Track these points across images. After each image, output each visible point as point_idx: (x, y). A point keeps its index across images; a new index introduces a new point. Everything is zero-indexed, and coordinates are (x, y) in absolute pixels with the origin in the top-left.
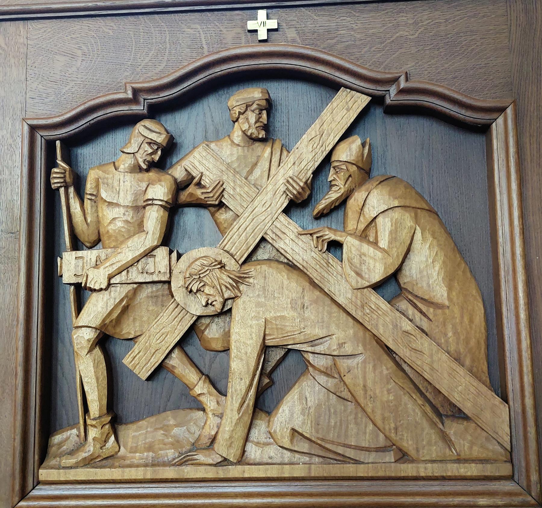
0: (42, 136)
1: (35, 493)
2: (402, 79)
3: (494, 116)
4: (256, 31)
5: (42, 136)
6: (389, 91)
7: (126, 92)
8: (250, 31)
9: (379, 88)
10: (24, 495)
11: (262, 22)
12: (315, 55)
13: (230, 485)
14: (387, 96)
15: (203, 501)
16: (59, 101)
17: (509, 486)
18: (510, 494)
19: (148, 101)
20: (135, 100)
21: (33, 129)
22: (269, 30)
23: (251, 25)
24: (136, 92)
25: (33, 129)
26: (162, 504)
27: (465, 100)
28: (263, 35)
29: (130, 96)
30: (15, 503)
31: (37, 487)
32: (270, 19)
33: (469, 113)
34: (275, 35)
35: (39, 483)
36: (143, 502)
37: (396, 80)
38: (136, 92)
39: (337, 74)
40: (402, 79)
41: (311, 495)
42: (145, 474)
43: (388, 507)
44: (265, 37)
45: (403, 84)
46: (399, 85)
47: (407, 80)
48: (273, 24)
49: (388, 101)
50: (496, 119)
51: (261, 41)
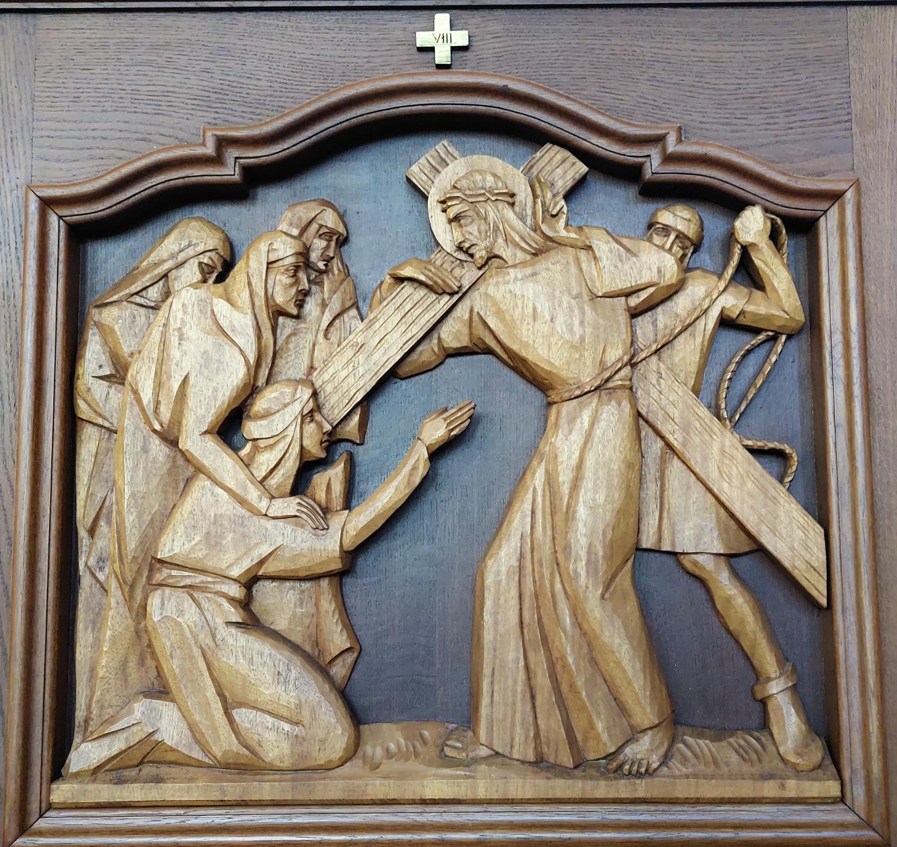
0: (60, 217)
1: (42, 824)
2: (671, 140)
3: (823, 206)
4: (432, 49)
6: (649, 156)
7: (204, 144)
8: (421, 50)
10: (24, 828)
11: (442, 34)
13: (293, 811)
14: (648, 164)
16: (86, 166)
17: (839, 814)
18: (843, 826)
19: (242, 161)
20: (217, 160)
21: (47, 204)
22: (454, 49)
23: (423, 39)
24: (223, 143)
25: (47, 204)
26: (788, 840)
27: (782, 179)
28: (442, 55)
29: (209, 150)
30: (10, 839)
31: (48, 814)
34: (459, 54)
35: (50, 807)
36: (674, 835)
37: (659, 140)
38: (223, 143)
42: (583, 790)
45: (672, 146)
46: (664, 149)
47: (679, 141)
48: (461, 38)
49: (648, 175)
50: (826, 211)
51: (440, 67)
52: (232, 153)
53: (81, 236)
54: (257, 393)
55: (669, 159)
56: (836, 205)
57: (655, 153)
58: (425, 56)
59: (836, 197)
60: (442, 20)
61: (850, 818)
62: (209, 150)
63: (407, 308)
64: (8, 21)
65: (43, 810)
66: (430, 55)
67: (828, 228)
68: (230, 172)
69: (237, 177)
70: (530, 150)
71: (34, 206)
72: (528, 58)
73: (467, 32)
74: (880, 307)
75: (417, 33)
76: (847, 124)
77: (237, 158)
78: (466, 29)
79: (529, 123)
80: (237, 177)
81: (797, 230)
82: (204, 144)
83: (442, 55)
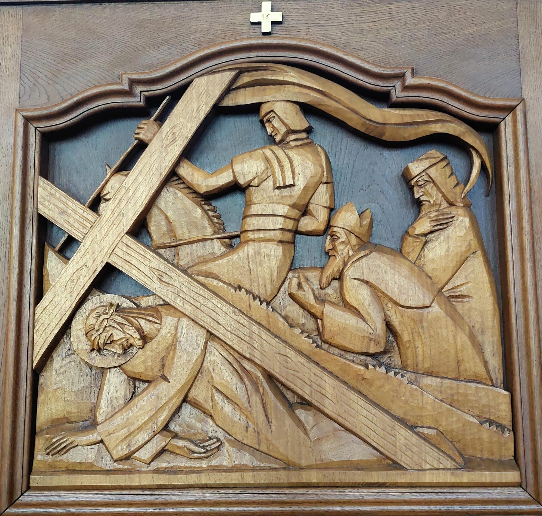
0: (36, 128)
1: (23, 499)
2: (409, 74)
3: (502, 115)
4: (259, 23)
5: (36, 128)
6: (394, 86)
7: (121, 83)
8: (253, 23)
9: (381, 84)
10: (12, 503)
12: (360, 64)
19: (144, 93)
20: (129, 93)
21: (28, 120)
23: (255, 17)
25: (28, 120)
28: (266, 28)
29: (126, 88)
31: (27, 493)
33: (469, 110)
34: (277, 27)
35: (28, 488)
37: (401, 76)
38: (133, 82)
39: (324, 61)
40: (409, 74)
43: (1, 464)
44: (269, 30)
45: (410, 81)
46: (404, 81)
47: (413, 75)
48: (278, 17)
49: (394, 98)
50: (504, 118)
51: (264, 34)
52: (138, 89)
53: (49, 139)
54: (287, 406)
55: (406, 88)
56: (511, 114)
57: (398, 84)
59: (511, 109)
61: (525, 496)
62: (126, 87)
65: (24, 490)
66: (259, 26)
67: (506, 130)
68: (138, 100)
69: (142, 104)
70: (323, 126)
71: (34, 138)
74: (535, 187)
75: (251, 14)
77: (141, 91)
80: (142, 104)
81: (489, 129)
82: (121, 83)
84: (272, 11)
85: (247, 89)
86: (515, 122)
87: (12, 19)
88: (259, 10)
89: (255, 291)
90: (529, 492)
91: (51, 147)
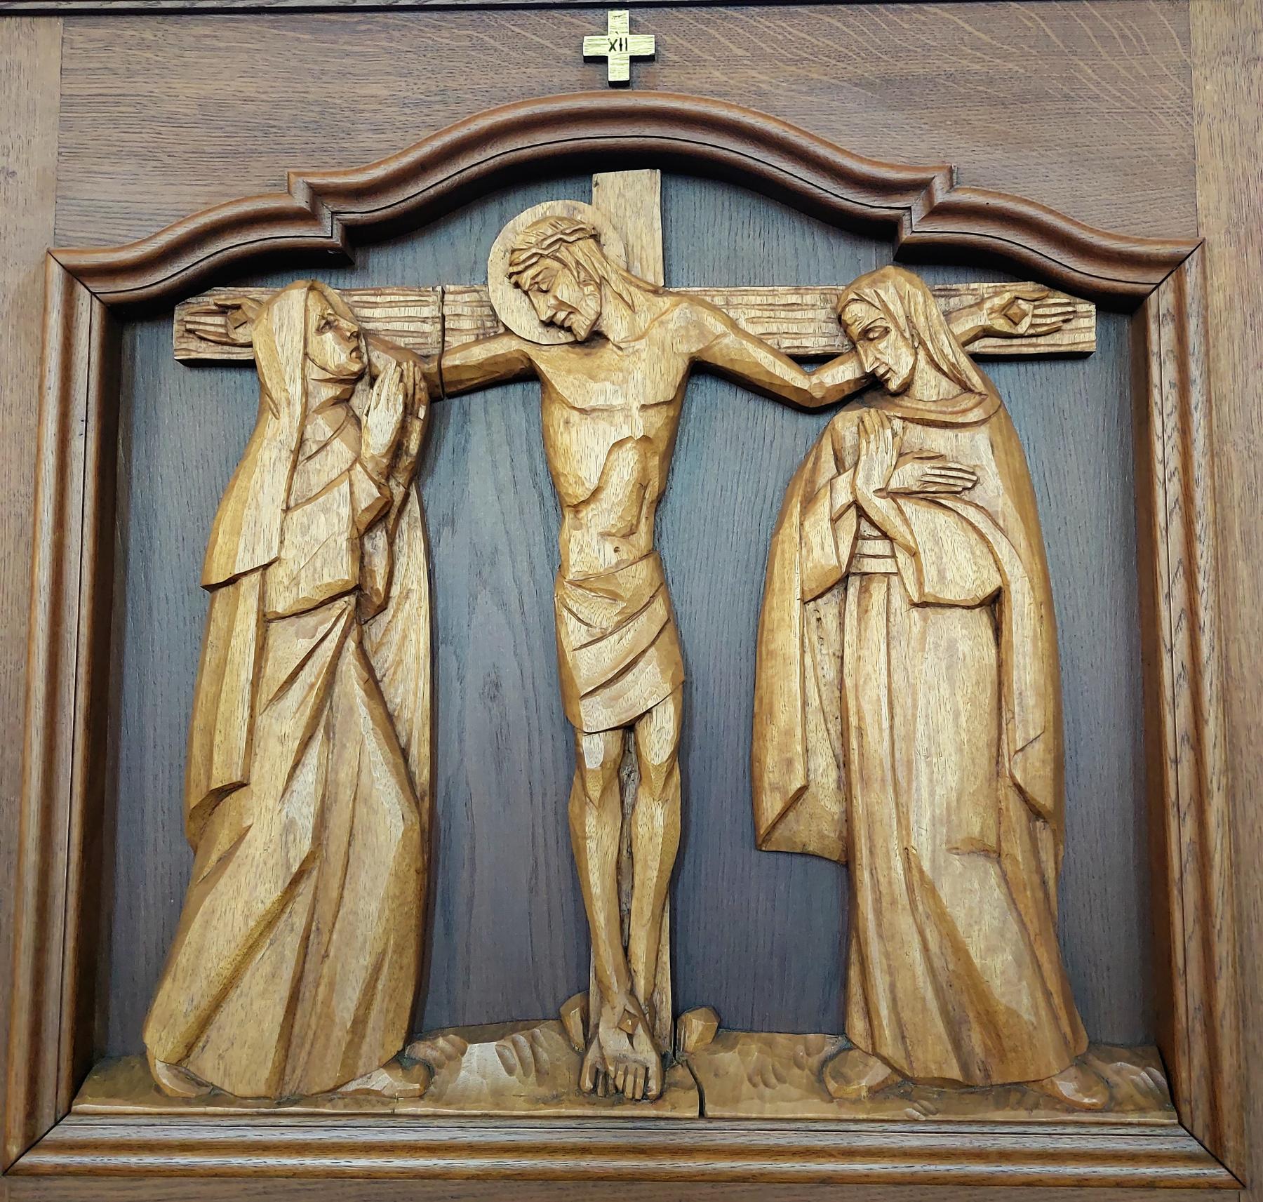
0: (93, 294)
1: (56, 1134)
2: (939, 183)
3: (1156, 277)
4: (603, 60)
5: (93, 294)
6: (909, 208)
10: (32, 1143)
11: (619, 39)
14: (906, 223)
15: (1087, 1170)
16: (146, 210)
21: (75, 275)
23: (594, 46)
24: (318, 193)
25: (75, 275)
28: (619, 70)
32: (639, 32)
34: (642, 67)
37: (923, 186)
38: (318, 193)
41: (1133, 1158)
43: (415, 1177)
45: (940, 197)
46: (930, 195)
47: (951, 188)
48: (644, 45)
49: (906, 235)
57: (917, 204)
58: (592, 69)
59: (1174, 264)
60: (618, 20)
62: (300, 200)
63: (985, 1130)
64: (698, 194)
67: (1162, 302)
68: (327, 232)
69: (337, 240)
72: (744, 74)
73: (651, 38)
76: (68, 92)
78: (654, 32)
79: (658, 146)
80: (337, 240)
83: (619, 70)
84: (631, 57)
85: (511, 388)
86: (1190, 1158)
87: (37, 49)
88: (604, 29)
89: (502, 1019)
90: (1229, 1165)
91: (127, 337)
